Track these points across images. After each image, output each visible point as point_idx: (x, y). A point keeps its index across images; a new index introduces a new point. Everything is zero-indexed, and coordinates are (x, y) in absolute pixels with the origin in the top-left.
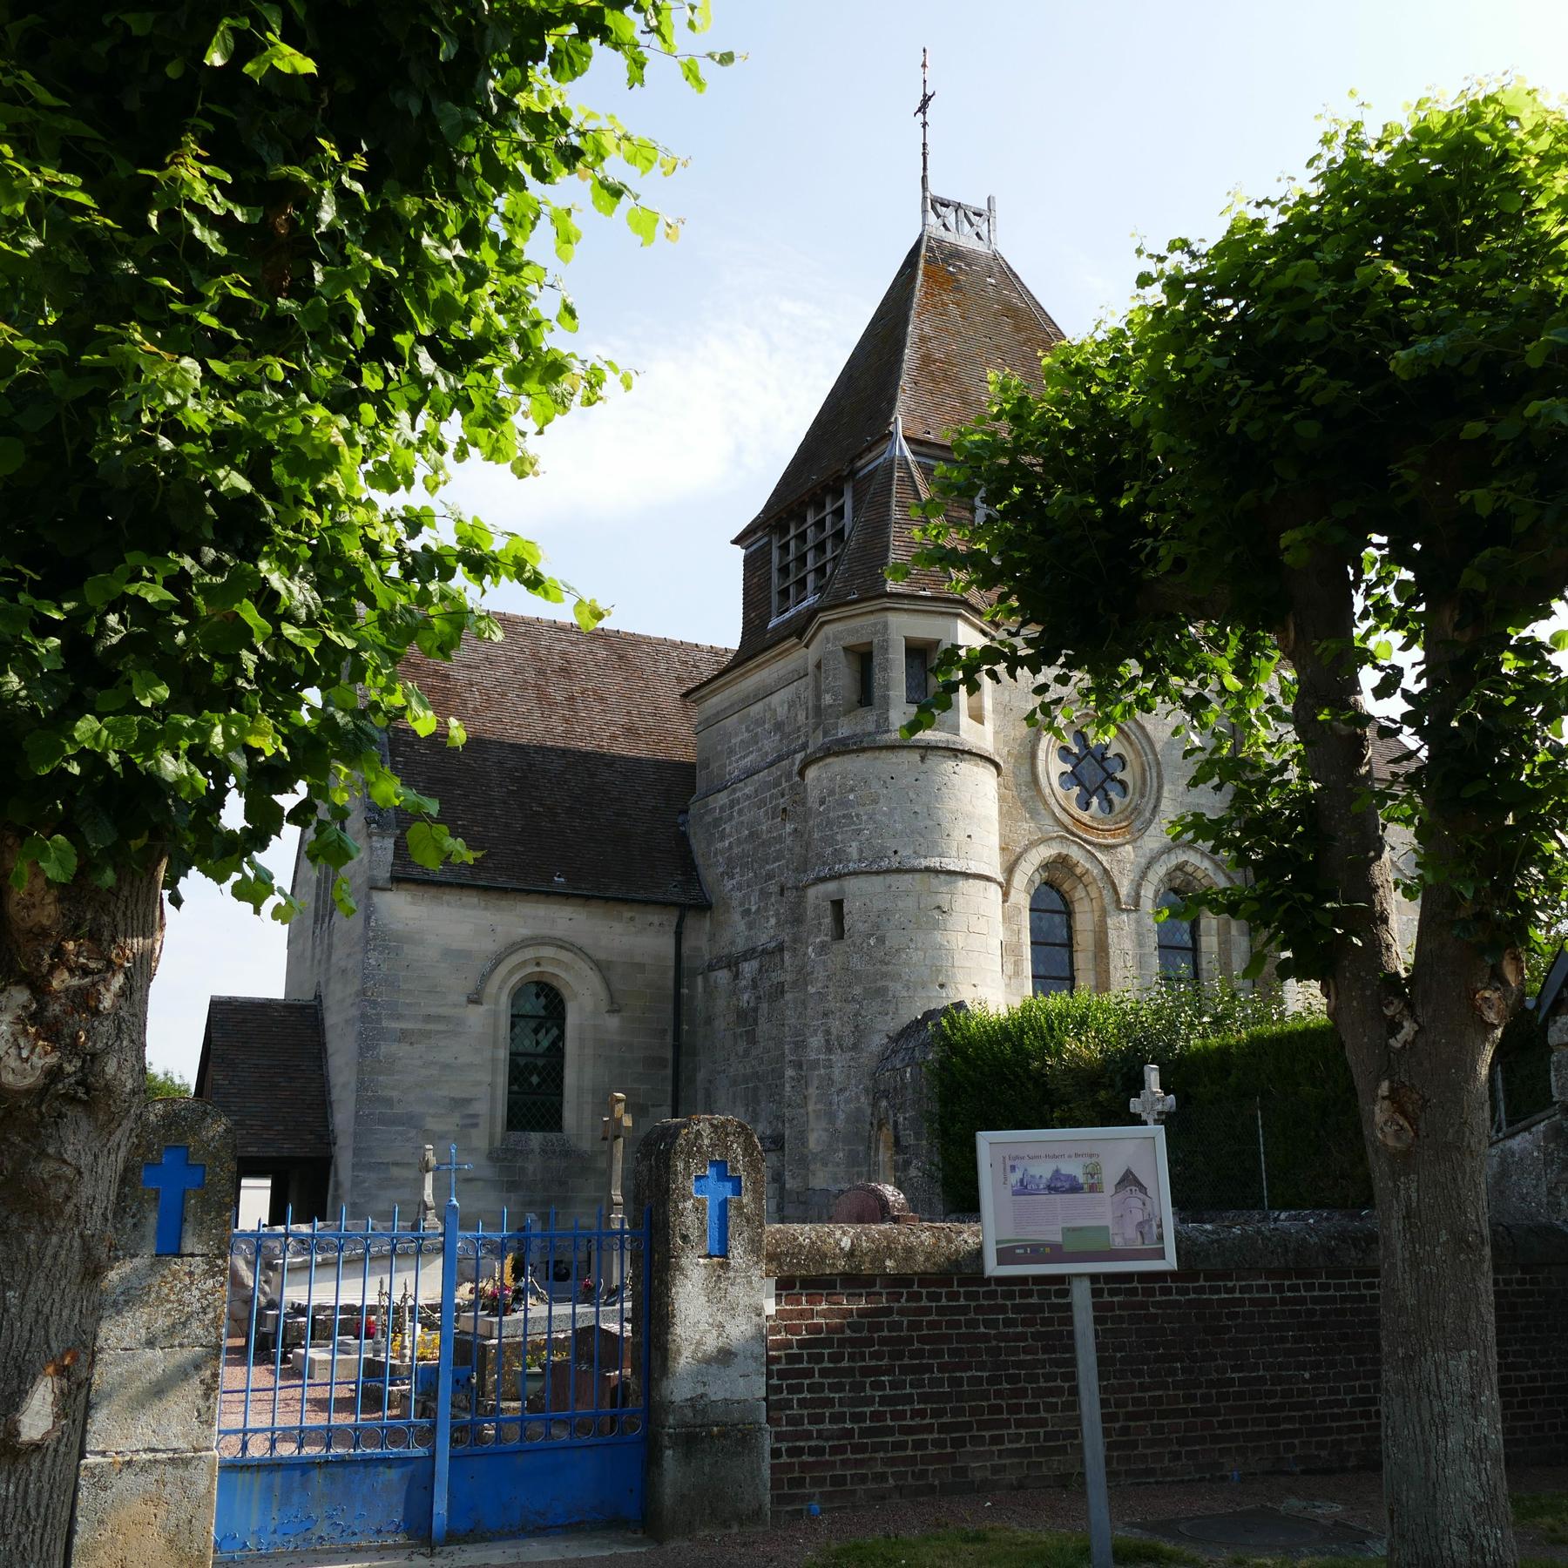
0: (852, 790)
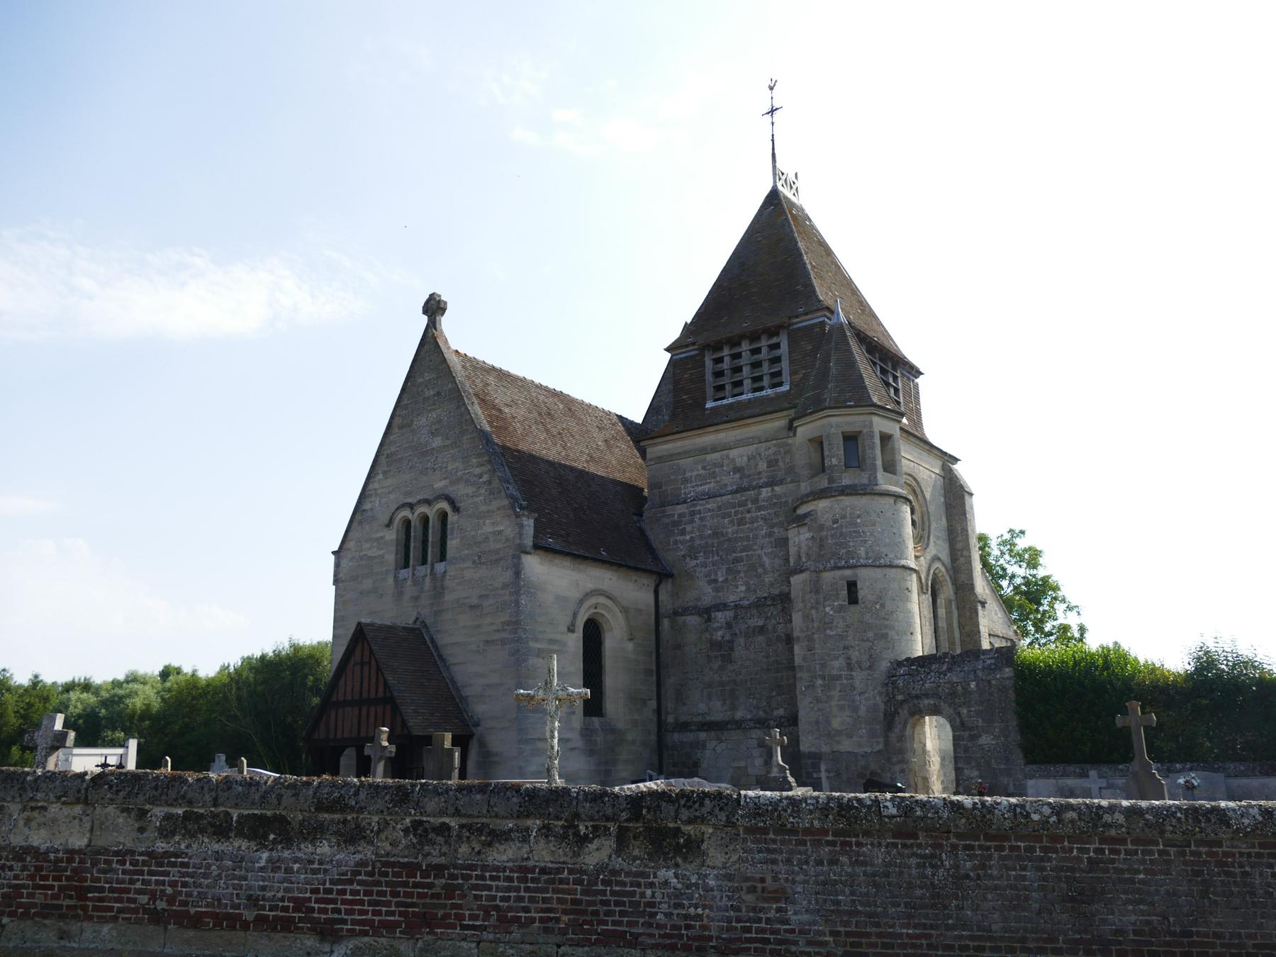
0: (859, 517)
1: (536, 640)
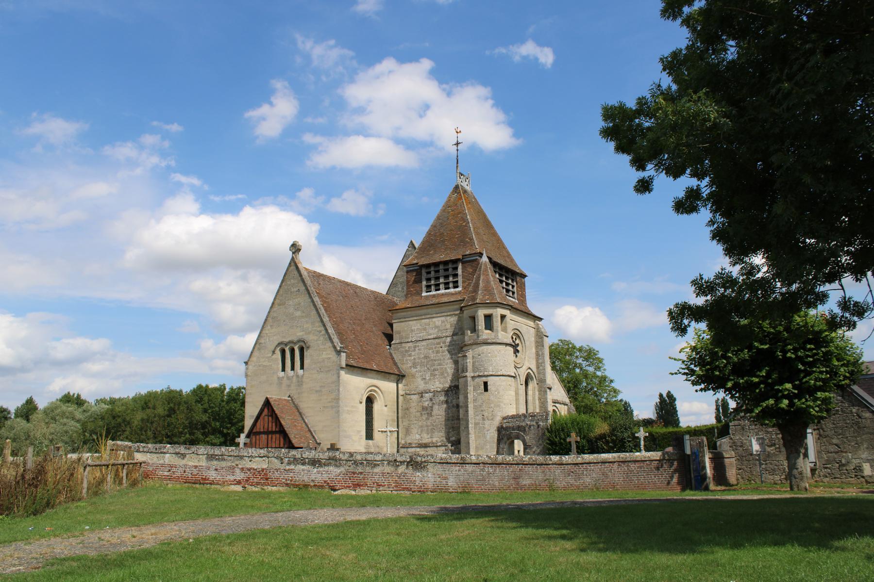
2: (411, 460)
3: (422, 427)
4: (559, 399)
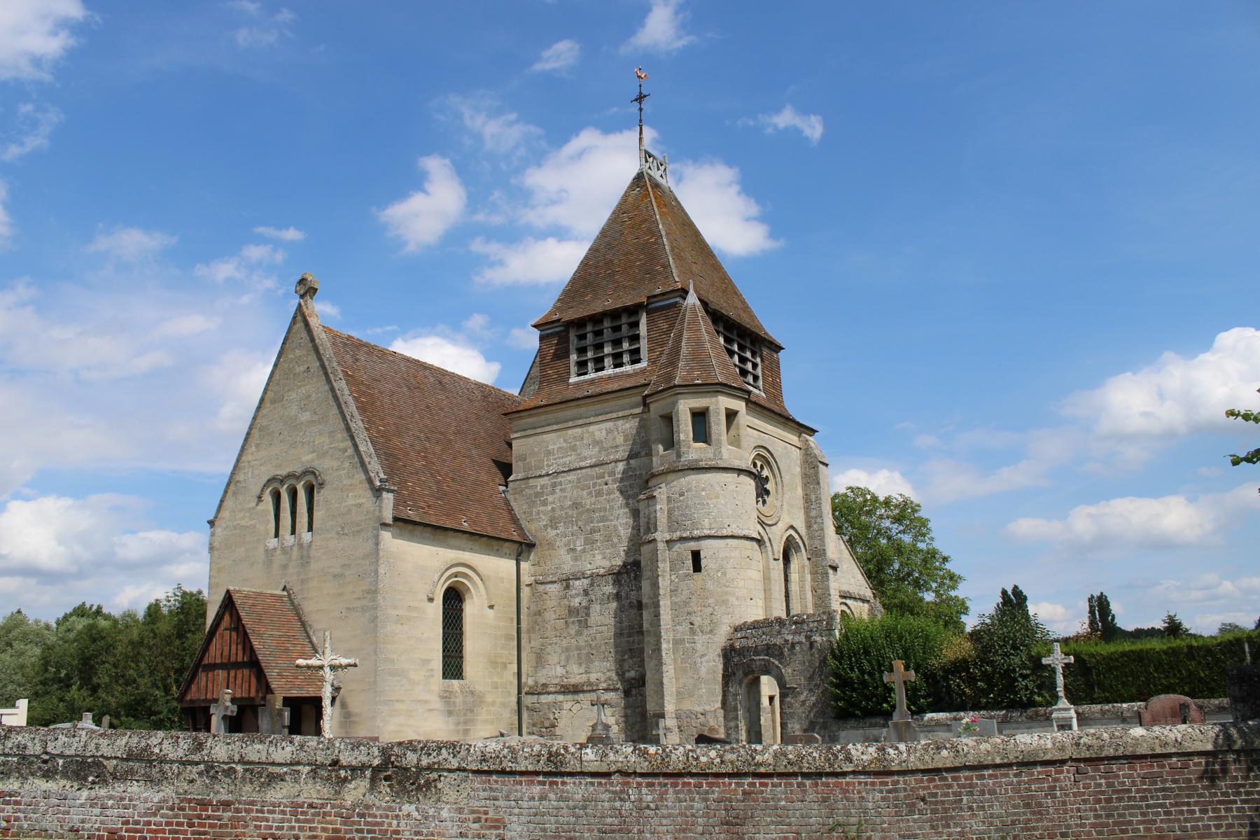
0: (703, 490)
1: (395, 608)
2: (386, 763)
3: (567, 649)
4: (854, 590)
